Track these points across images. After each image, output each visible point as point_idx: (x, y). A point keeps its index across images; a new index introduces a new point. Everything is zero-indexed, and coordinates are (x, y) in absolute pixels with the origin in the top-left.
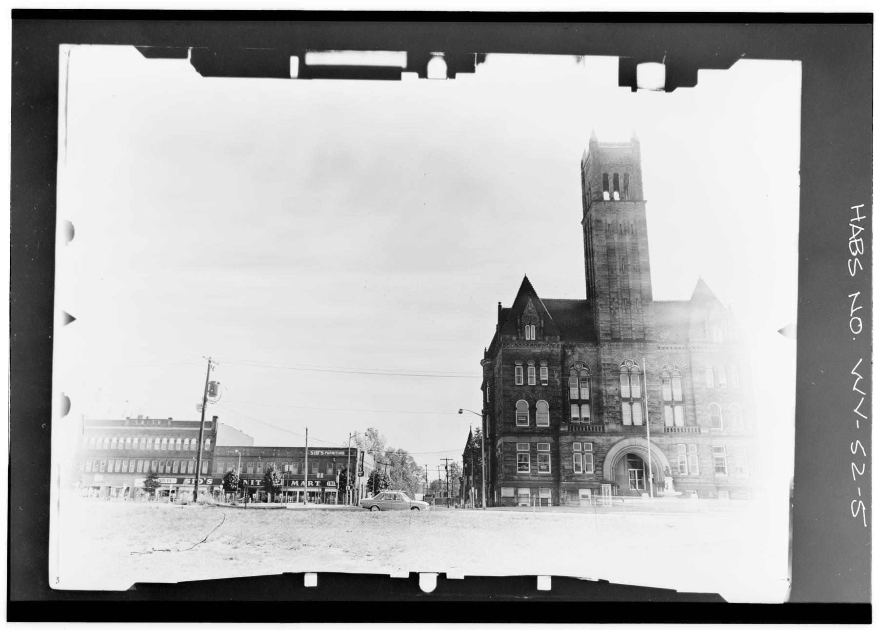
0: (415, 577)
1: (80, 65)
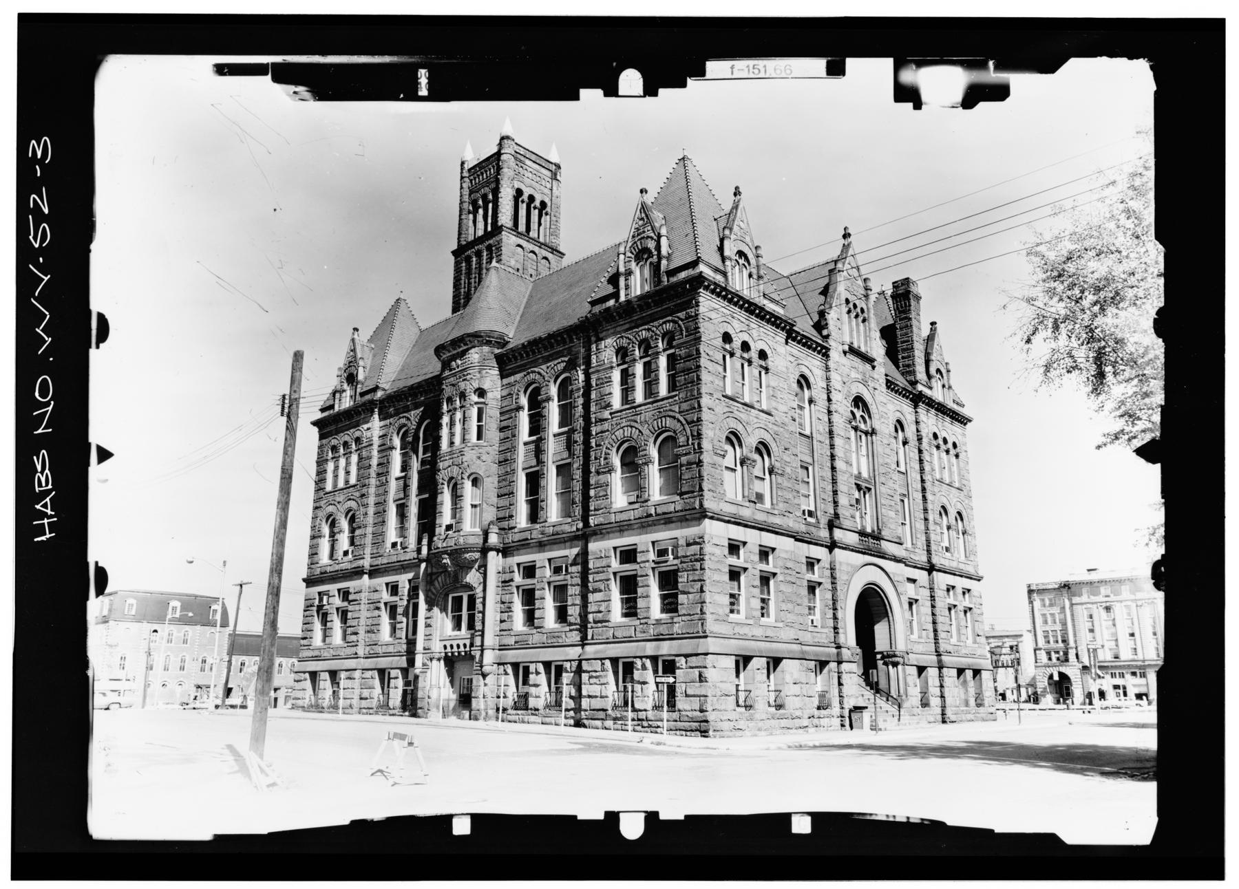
0: (612, 818)
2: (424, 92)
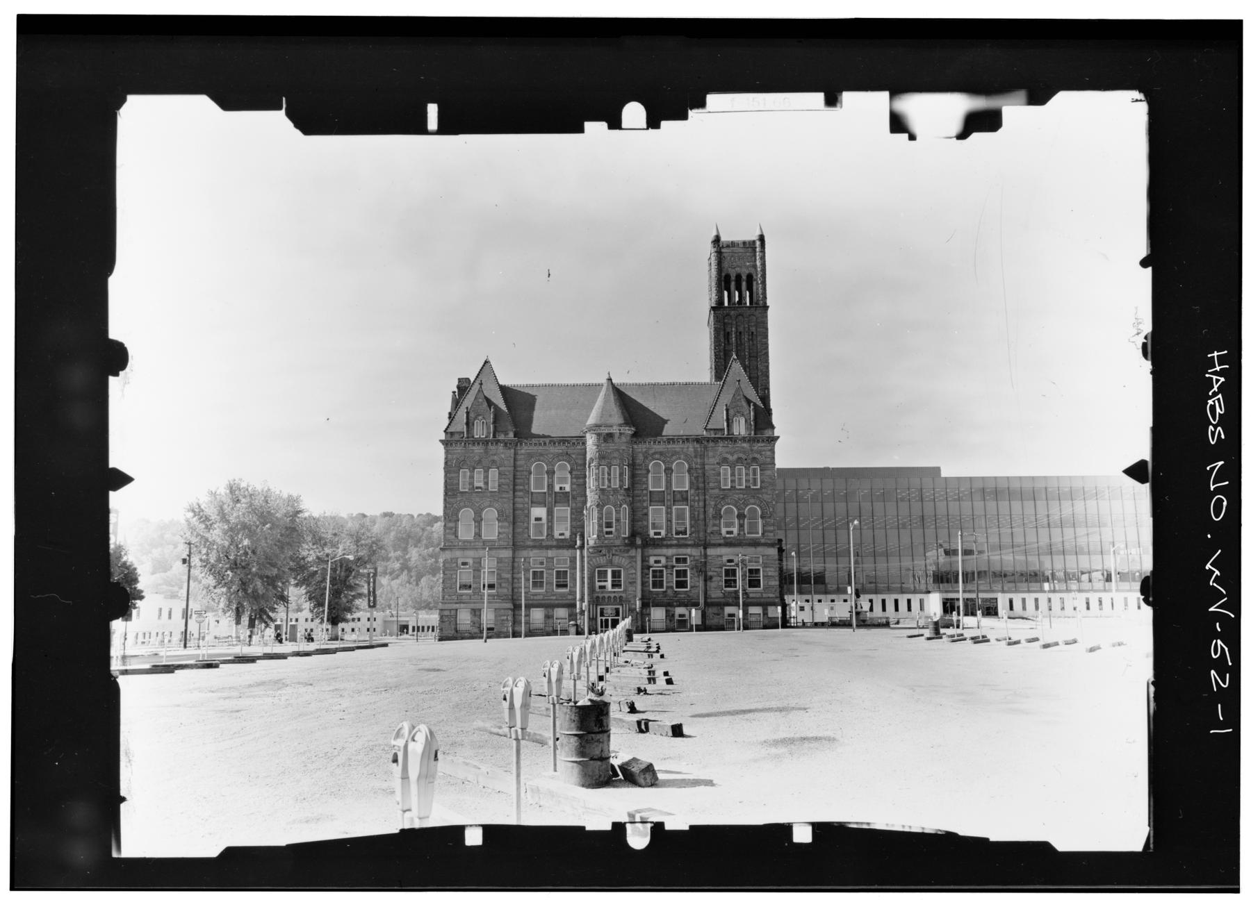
0: (653, 122)
1: (163, 141)
2: (433, 123)
